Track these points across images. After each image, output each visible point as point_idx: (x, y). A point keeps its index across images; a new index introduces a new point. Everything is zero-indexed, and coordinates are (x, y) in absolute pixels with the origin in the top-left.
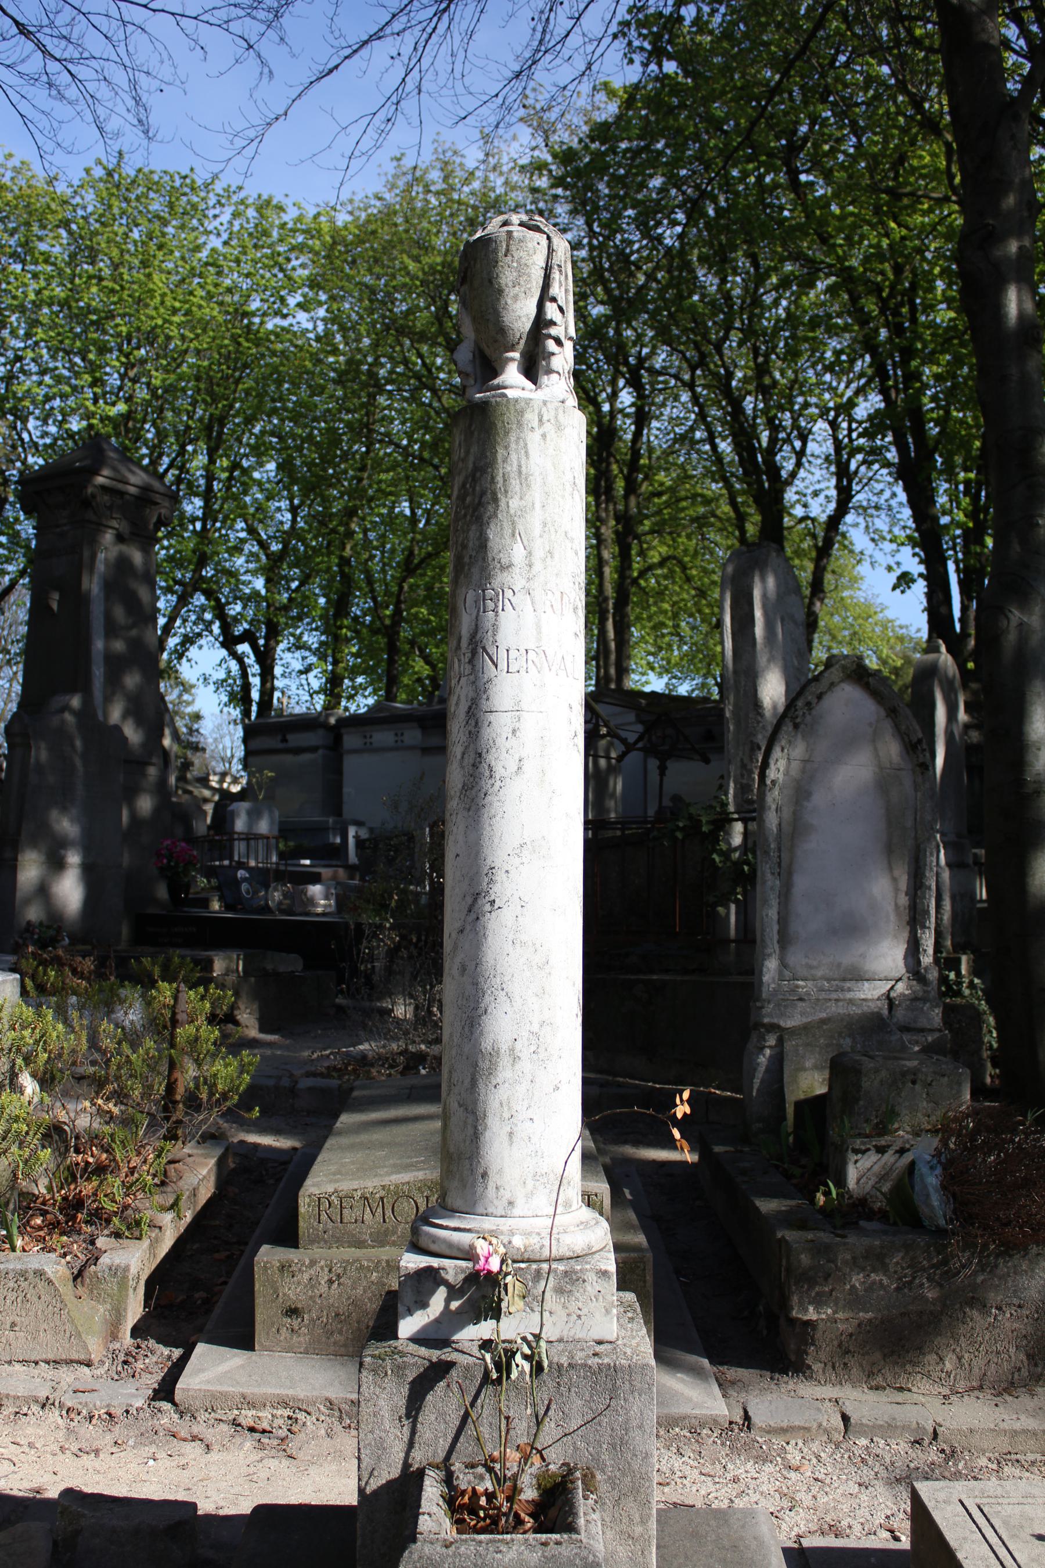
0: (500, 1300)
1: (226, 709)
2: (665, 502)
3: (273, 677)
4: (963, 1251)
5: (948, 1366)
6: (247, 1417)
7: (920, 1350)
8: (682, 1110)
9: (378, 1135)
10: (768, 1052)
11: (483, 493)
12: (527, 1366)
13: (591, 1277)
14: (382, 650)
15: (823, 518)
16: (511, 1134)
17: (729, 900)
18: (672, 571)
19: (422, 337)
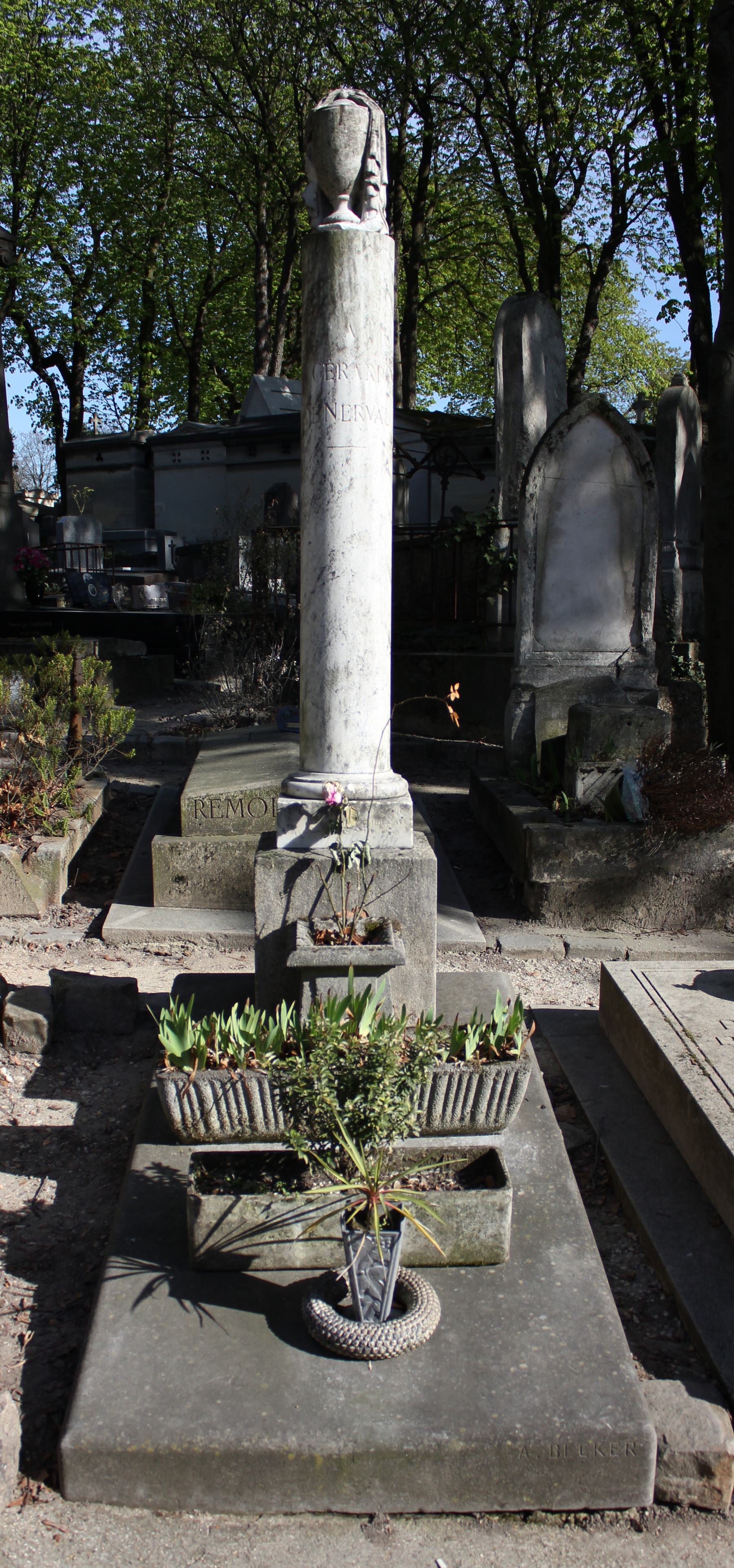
0: (341, 822)
1: (38, 430)
2: (450, 228)
3: (83, 398)
4: (654, 836)
5: (640, 915)
6: (154, 946)
7: (621, 904)
8: (454, 695)
9: (231, 762)
10: (523, 706)
11: (326, 297)
12: (358, 861)
13: (397, 809)
14: (183, 371)
15: (599, 245)
16: (346, 722)
17: (497, 591)
18: (456, 297)
19: (216, 61)
